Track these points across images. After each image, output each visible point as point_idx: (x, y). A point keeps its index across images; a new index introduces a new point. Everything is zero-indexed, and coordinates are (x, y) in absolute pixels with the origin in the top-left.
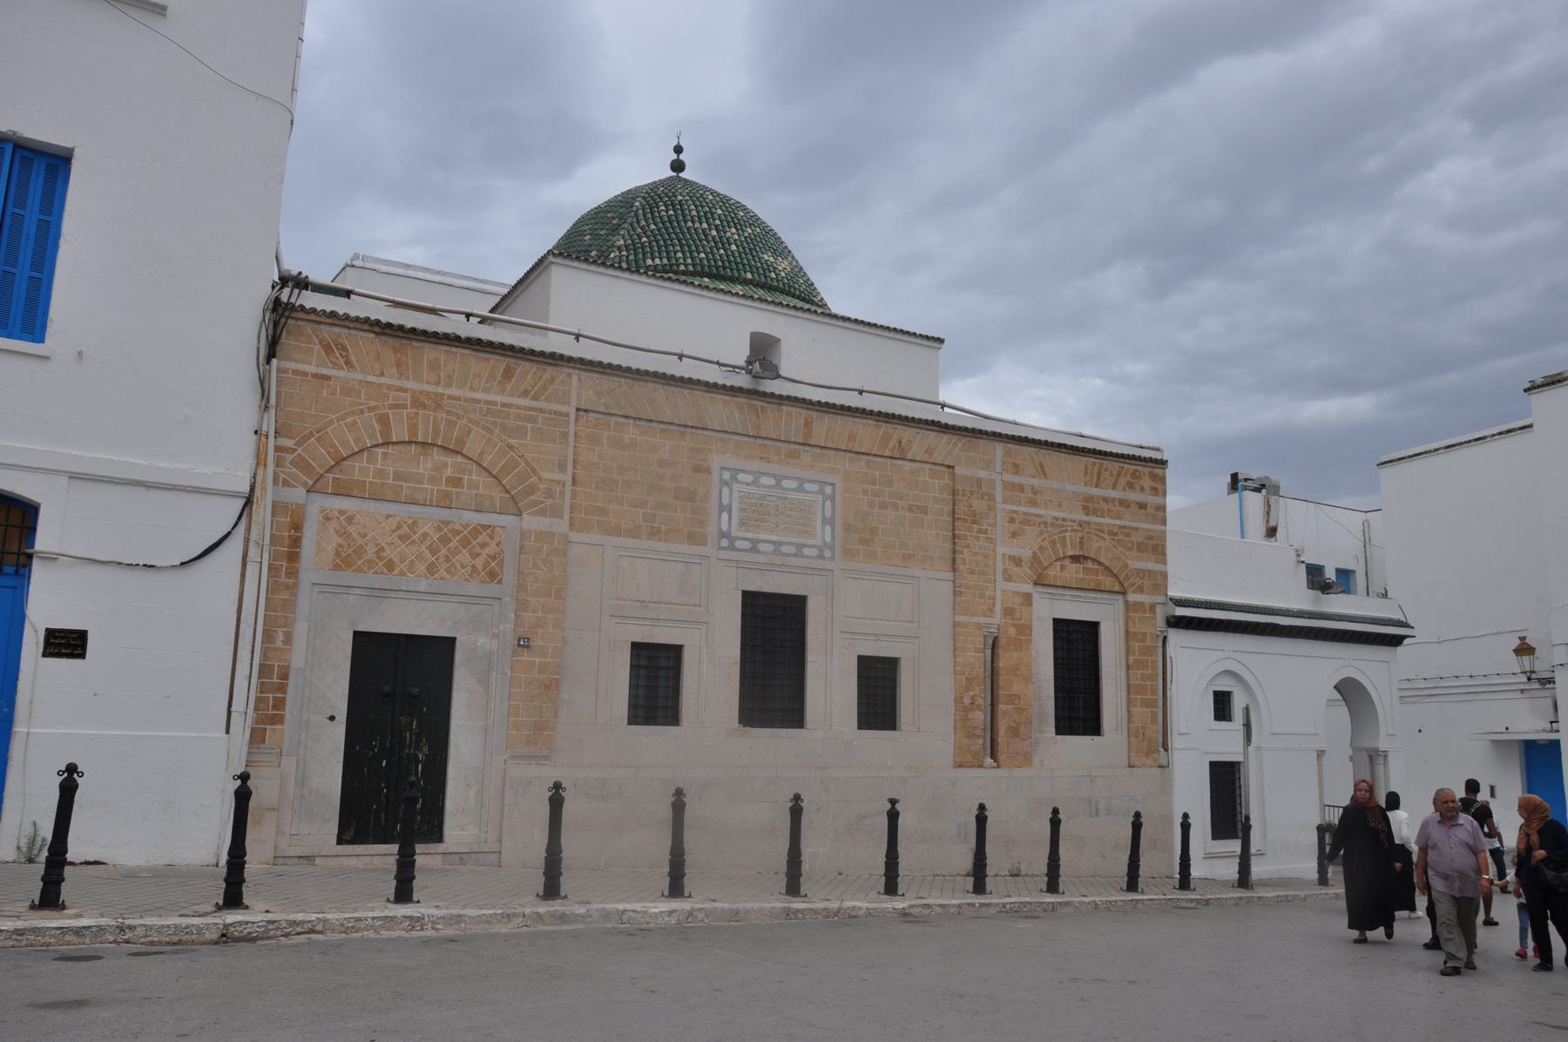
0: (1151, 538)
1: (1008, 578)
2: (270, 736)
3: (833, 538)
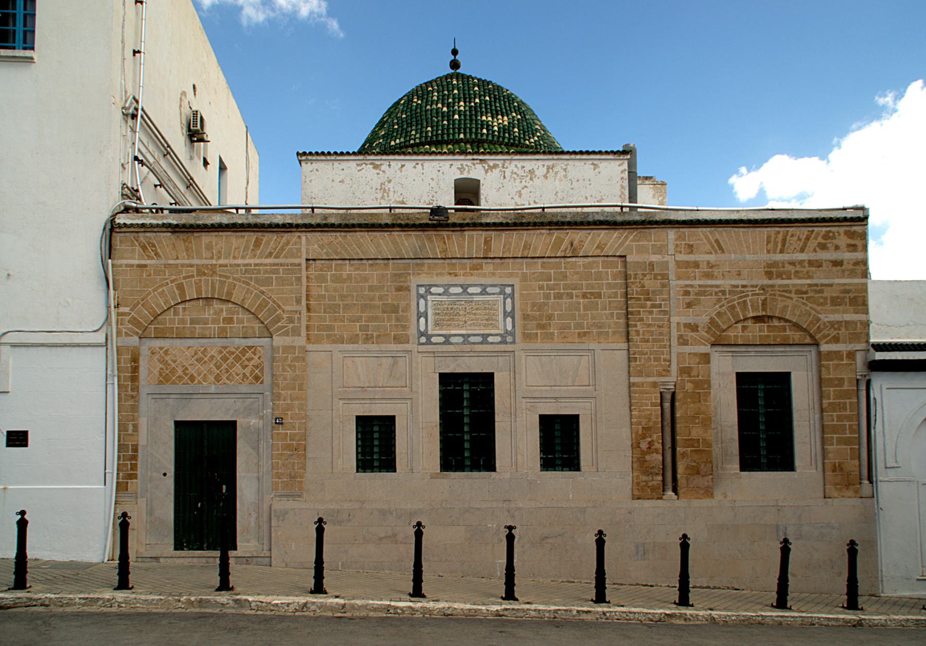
0: (849, 291)
1: (683, 341)
3: (514, 326)
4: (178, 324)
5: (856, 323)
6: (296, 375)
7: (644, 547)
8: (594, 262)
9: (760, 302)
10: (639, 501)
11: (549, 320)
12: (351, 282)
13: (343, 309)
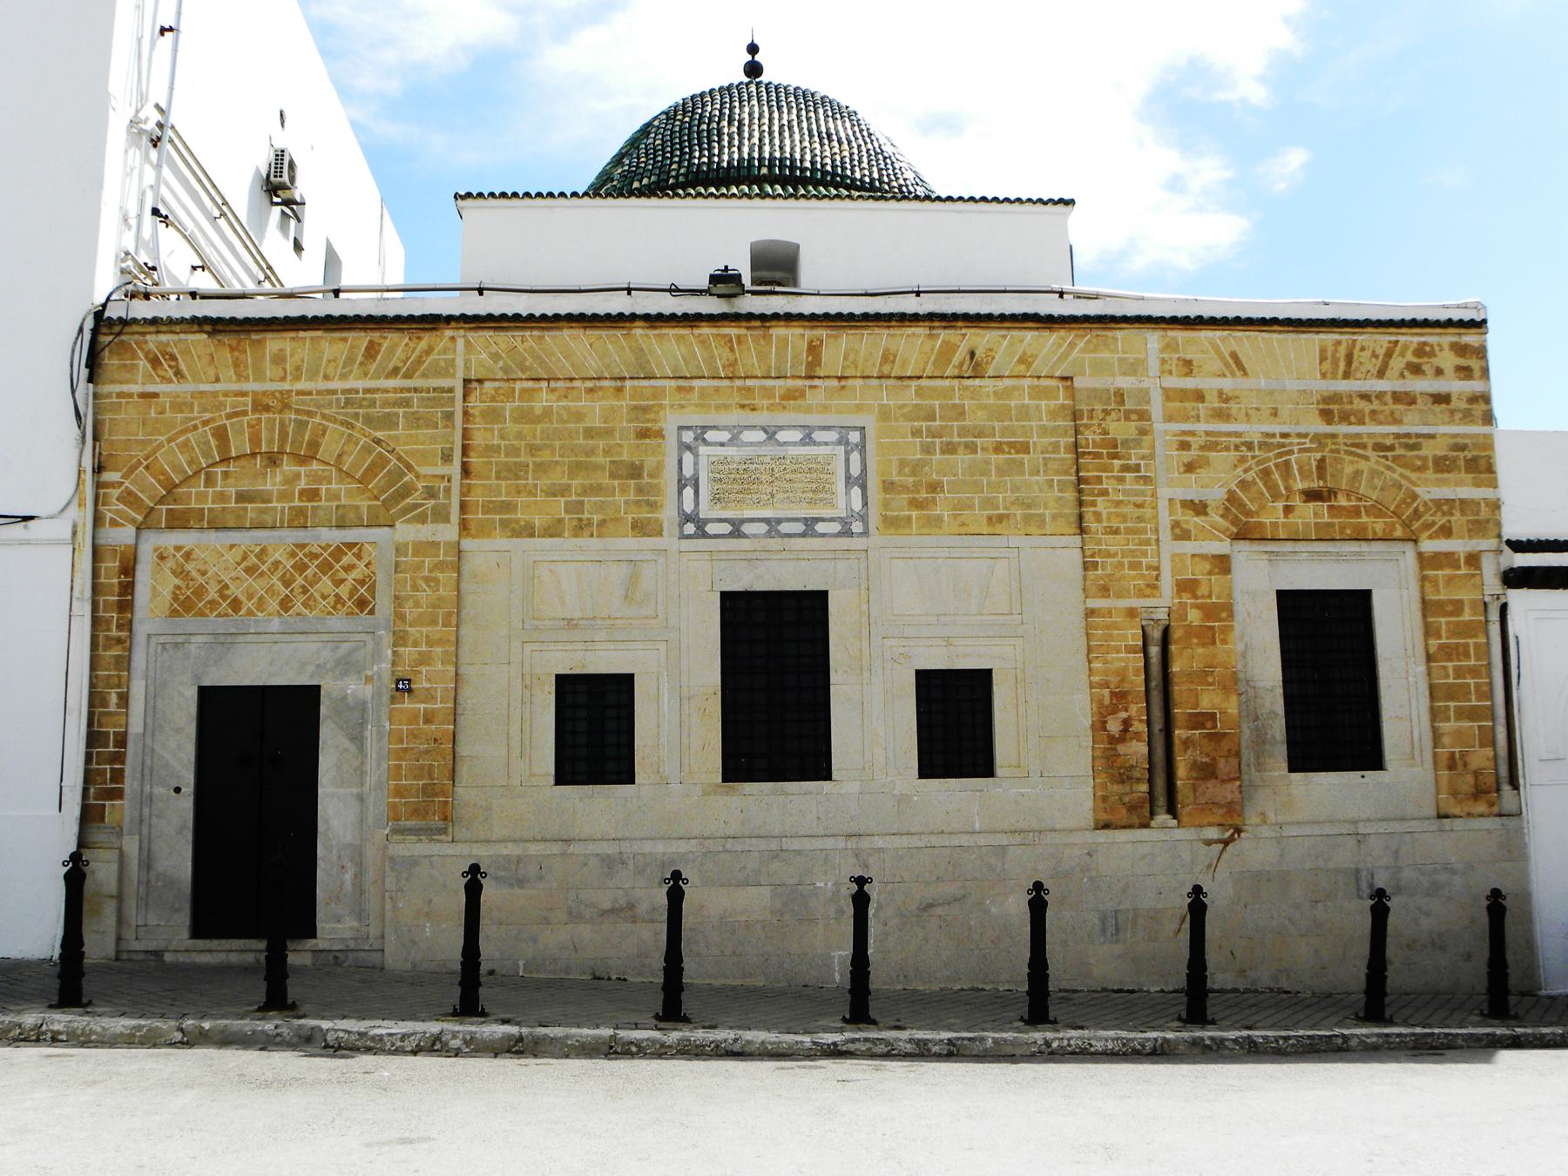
0: (1463, 448)
1: (1181, 534)
2: (110, 813)
3: (865, 504)
4: (213, 502)
5: (1479, 503)
6: (440, 598)
7: (1116, 918)
8: (1014, 388)
9: (1314, 464)
10: (1106, 831)
11: (933, 492)
12: (551, 421)
13: (534, 471)
